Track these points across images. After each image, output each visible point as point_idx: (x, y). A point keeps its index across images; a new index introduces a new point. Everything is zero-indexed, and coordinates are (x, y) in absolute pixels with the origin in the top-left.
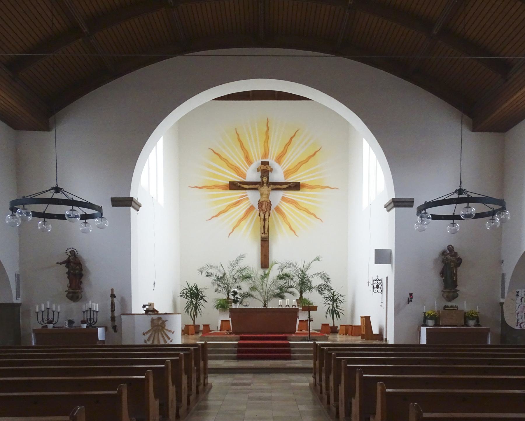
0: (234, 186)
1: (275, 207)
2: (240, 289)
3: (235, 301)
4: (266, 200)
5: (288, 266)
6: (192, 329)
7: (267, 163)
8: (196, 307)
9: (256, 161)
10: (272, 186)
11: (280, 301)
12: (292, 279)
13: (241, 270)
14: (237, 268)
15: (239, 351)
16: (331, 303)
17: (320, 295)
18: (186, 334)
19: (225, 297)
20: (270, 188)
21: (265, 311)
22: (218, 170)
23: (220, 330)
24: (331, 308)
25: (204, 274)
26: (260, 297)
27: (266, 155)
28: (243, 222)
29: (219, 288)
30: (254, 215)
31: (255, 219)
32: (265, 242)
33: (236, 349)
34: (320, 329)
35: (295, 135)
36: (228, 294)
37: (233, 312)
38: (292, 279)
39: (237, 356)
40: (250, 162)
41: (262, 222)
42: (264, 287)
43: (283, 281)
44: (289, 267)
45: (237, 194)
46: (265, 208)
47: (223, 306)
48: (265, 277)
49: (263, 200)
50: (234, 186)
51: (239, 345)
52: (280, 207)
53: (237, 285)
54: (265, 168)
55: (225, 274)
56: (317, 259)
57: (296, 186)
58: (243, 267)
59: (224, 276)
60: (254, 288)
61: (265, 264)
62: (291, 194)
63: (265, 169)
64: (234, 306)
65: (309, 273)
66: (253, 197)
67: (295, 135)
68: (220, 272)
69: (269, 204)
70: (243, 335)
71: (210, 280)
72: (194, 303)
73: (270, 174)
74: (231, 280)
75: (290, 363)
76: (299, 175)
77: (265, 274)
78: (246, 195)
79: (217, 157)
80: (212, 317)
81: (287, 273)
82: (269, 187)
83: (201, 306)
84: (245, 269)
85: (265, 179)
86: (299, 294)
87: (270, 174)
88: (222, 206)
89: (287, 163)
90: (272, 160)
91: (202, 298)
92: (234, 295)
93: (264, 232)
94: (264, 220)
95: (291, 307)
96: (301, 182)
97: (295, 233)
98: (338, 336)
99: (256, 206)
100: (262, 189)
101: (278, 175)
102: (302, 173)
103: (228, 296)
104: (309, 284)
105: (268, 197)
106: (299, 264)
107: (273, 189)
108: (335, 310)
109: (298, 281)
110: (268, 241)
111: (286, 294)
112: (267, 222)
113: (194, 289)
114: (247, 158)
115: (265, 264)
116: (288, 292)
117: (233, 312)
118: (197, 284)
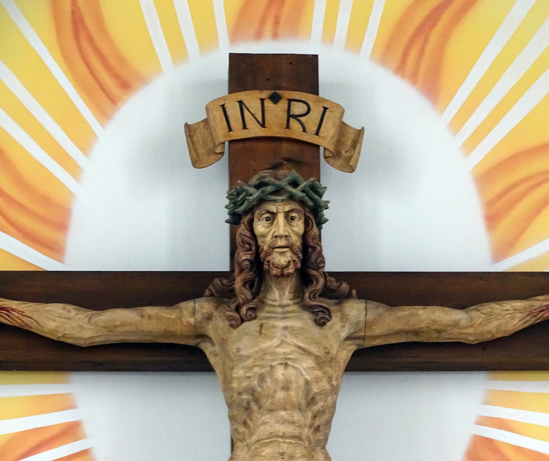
7: (302, 72)
10: (355, 310)
40: (107, 76)
54: (275, 129)
63: (275, 138)
73: (333, 181)
78: (70, 431)
82: (322, 319)
85: (278, 229)
90: (354, 43)
100: (245, 342)
107: (372, 359)
114: (78, 22)
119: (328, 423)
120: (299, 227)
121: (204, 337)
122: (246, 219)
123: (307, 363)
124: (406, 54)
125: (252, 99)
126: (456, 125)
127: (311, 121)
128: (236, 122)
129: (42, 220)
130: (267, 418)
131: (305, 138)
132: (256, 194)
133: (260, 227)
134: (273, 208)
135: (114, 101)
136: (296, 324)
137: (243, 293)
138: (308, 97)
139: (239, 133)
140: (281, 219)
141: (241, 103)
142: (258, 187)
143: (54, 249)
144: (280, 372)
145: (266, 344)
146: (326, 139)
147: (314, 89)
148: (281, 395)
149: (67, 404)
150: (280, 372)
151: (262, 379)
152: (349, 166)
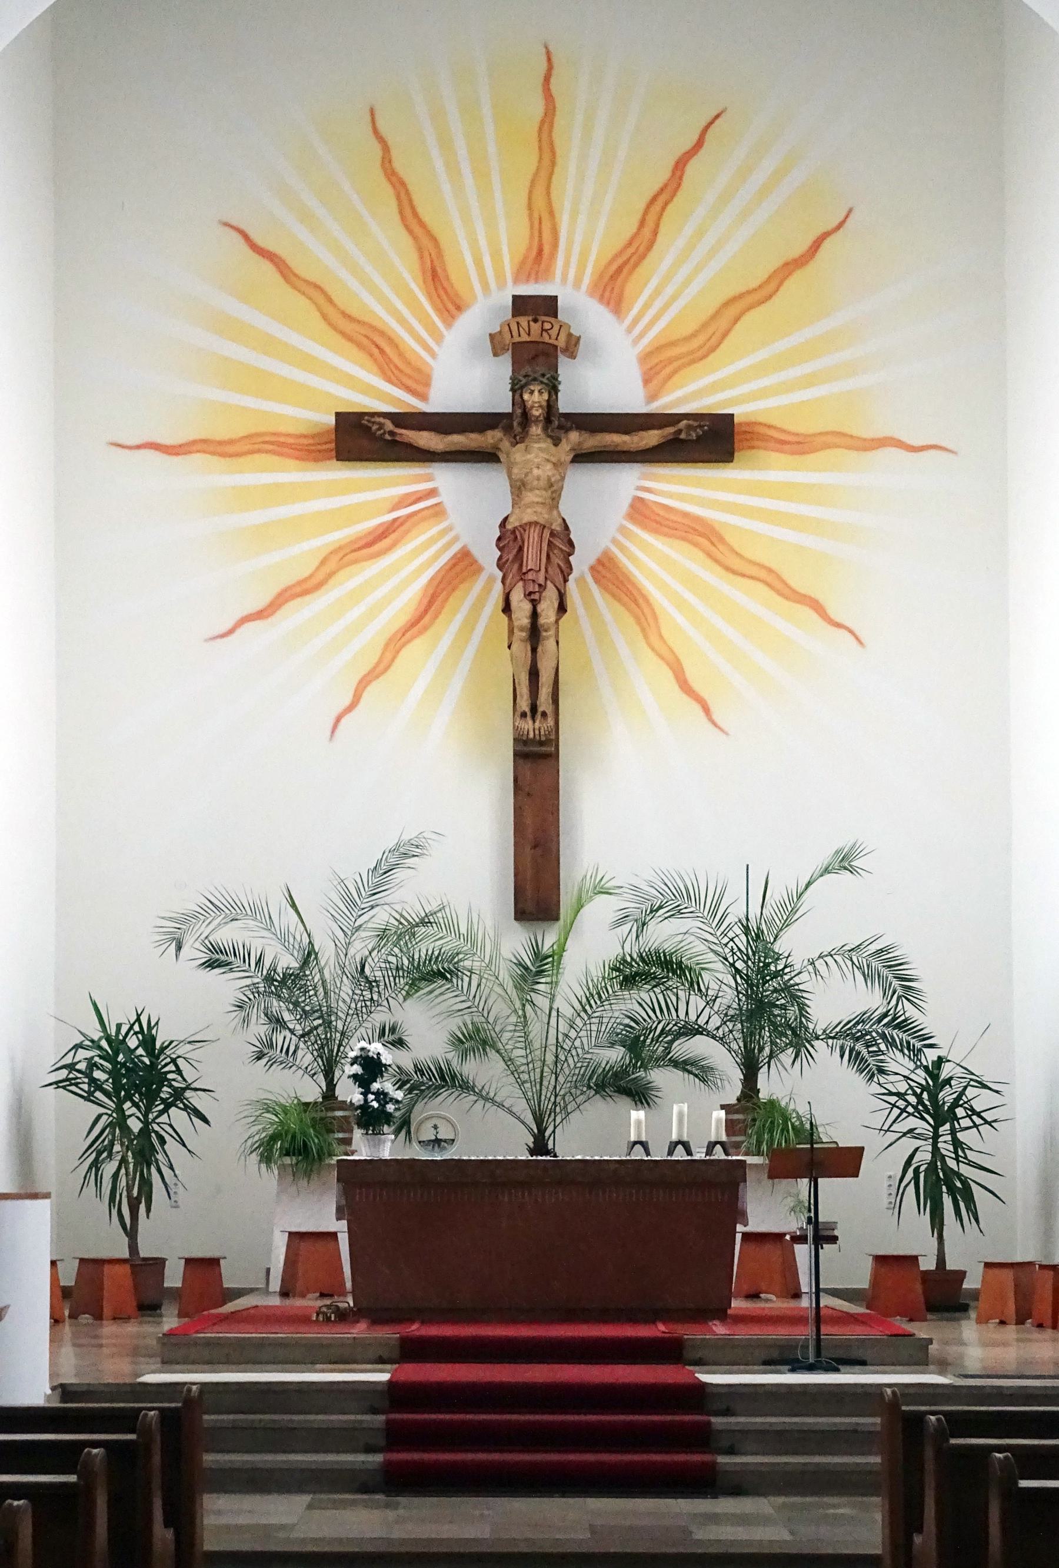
0: (360, 439)
1: (592, 561)
2: (400, 1043)
3: (372, 1119)
4: (543, 516)
5: (674, 902)
6: (116, 1281)
7: (548, 306)
8: (145, 1150)
10: (574, 436)
11: (638, 1115)
12: (694, 985)
13: (406, 931)
14: (381, 917)
15: (396, 1437)
16: (922, 1127)
17: (860, 1080)
18: (85, 1318)
19: (312, 1091)
20: (565, 446)
21: (541, 1176)
22: (268, 345)
23: (284, 1294)
24: (925, 1156)
25: (194, 951)
26: (508, 1091)
27: (538, 258)
28: (416, 648)
29: (278, 1038)
30: (469, 625)
31: (480, 629)
32: (536, 764)
33: (379, 1419)
34: (865, 1284)
35: (699, 144)
36: (329, 1074)
37: (360, 1183)
38: (694, 985)
39: (388, 1465)
40: (449, 302)
41: (521, 649)
42: (536, 1029)
43: (645, 994)
44: (678, 912)
45: (378, 488)
46: (535, 563)
47: (297, 1144)
48: (538, 969)
49: (528, 516)
50: (360, 439)
51: (396, 1395)
53: (380, 1017)
54: (535, 336)
55: (309, 956)
56: (844, 862)
57: (711, 439)
58: (415, 912)
59: (305, 963)
60: (475, 1040)
61: (537, 893)
62: (679, 486)
63: (535, 341)
64: (363, 1148)
65: (795, 946)
66: (469, 503)
67: (699, 144)
68: (283, 940)
69: (561, 542)
70: (415, 1329)
71: (228, 987)
72: (135, 1125)
74: (347, 988)
75: (714, 1519)
76: (731, 369)
77: (539, 957)
78: (432, 493)
79: (267, 266)
80: (239, 1210)
81: (668, 947)
82: (556, 442)
83: (171, 1145)
84: (424, 922)
85: (535, 398)
86: (736, 1075)
87: (566, 369)
88: (301, 555)
89: (658, 304)
90: (577, 285)
91: (178, 1095)
92: (363, 1081)
93: (534, 709)
94: (535, 633)
95: (659, 1154)
96: (740, 412)
97: (707, 710)
98: (969, 1329)
99: (488, 555)
100: (518, 454)
101: (605, 378)
102: (741, 364)
103: (331, 1085)
104: (792, 1012)
105: (554, 501)
106: (735, 892)
107: (582, 457)
108: (945, 1168)
109: (728, 997)
110: (554, 756)
111: (660, 1077)
112: (548, 645)
113: (132, 1042)
115: (537, 893)
116: (676, 1064)
117: (360, 1183)
118: (152, 1012)
119: (560, 495)
120: (546, 396)
121: (499, 449)
122: (519, 392)
123: (549, 466)
124: (604, 291)
125: (524, 321)
126: (629, 330)
127: (554, 332)
128: (515, 333)
129: (416, 381)
130: (529, 494)
131: (550, 341)
132: (524, 381)
133: (526, 397)
134: (532, 388)
135: (453, 317)
136: (543, 445)
137: (517, 428)
138: (552, 320)
139: (517, 339)
140: (536, 393)
141: (518, 323)
142: (525, 376)
143: (423, 397)
144: (536, 472)
145: (529, 456)
146: (561, 342)
147: (556, 316)
148: (535, 483)
149: (430, 478)
150: (536, 472)
151: (526, 475)
152: (573, 356)
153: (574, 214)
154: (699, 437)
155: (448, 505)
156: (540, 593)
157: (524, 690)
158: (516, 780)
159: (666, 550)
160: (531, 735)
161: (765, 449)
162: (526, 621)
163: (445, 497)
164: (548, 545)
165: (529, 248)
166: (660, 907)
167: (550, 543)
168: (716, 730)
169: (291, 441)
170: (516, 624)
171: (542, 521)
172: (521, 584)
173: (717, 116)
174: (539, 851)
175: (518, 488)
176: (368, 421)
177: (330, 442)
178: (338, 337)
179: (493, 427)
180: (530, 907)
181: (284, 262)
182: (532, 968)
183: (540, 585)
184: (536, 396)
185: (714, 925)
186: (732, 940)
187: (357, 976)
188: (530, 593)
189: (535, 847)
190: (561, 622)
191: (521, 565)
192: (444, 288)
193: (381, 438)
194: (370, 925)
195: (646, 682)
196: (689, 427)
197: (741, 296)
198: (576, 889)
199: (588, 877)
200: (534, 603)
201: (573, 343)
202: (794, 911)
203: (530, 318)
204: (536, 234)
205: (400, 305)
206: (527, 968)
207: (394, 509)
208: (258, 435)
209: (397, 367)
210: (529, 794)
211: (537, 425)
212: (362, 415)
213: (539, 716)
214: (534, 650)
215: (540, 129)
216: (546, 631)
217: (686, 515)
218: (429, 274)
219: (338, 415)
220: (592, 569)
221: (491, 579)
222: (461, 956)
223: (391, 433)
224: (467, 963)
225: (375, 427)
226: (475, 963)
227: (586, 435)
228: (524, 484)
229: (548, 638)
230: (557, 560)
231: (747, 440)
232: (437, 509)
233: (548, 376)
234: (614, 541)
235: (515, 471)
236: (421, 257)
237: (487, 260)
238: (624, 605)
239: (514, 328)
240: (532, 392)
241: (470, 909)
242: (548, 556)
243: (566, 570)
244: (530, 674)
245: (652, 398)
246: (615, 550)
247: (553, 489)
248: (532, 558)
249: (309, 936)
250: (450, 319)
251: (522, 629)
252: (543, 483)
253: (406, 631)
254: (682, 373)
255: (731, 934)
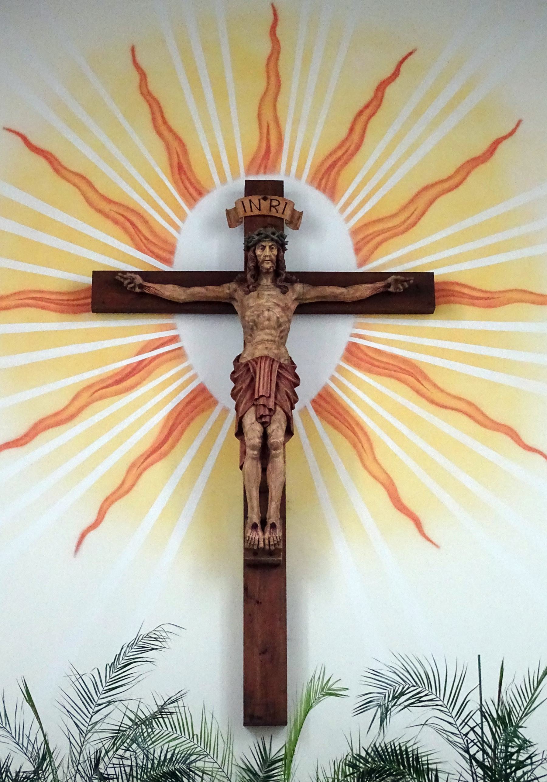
0: (114, 294)
1: (313, 395)
9: (224, 181)
10: (299, 287)
14: (115, 717)
20: (291, 296)
22: (41, 223)
27: (267, 155)
28: (156, 472)
32: (265, 575)
41: (252, 467)
45: (128, 335)
46: (265, 393)
50: (114, 294)
52: (339, 392)
57: (415, 295)
58: (149, 708)
61: (266, 697)
62: (388, 334)
63: (264, 215)
66: (206, 348)
69: (287, 375)
77: (268, 762)
78: (174, 339)
79: (42, 163)
82: (284, 292)
85: (266, 253)
88: (56, 391)
90: (299, 176)
93: (263, 522)
96: (440, 273)
99: (222, 388)
100: (251, 301)
101: (325, 243)
107: (305, 309)
114: (180, 167)
115: (266, 697)
119: (287, 335)
120: (275, 252)
121: (234, 299)
122: (252, 249)
123: (277, 310)
125: (255, 199)
127: (280, 208)
130: (260, 332)
131: (277, 215)
132: (257, 238)
133: (258, 252)
134: (264, 244)
135: (195, 200)
136: (272, 293)
139: (249, 213)
140: (267, 248)
141: (250, 201)
144: (266, 314)
146: (287, 216)
148: (266, 323)
149: (173, 327)
150: (266, 314)
151: (258, 316)
153: (296, 122)
154: (405, 290)
155: (188, 350)
156: (271, 416)
157: (255, 503)
158: (246, 589)
159: (378, 386)
160: (262, 545)
161: (460, 303)
162: (257, 441)
163: (184, 343)
164: (278, 375)
165: (259, 147)
166: (402, 694)
167: (279, 375)
168: (428, 543)
169: (53, 297)
170: (248, 443)
171: (272, 355)
172: (253, 409)
173: (410, 54)
174: (267, 656)
175: (250, 330)
176: (121, 277)
177: (88, 298)
178: (97, 216)
179: (230, 281)
180: (259, 711)
181: (56, 159)
182: (261, 774)
183: (270, 410)
184: (267, 251)
185: (454, 714)
186: (472, 729)
187: (90, 772)
188: (262, 417)
189: (263, 652)
190: (287, 444)
191: (253, 394)
192: (189, 180)
193: (131, 292)
194: (105, 726)
195: (365, 500)
196: (396, 281)
197: (432, 185)
198: (305, 689)
199: (317, 678)
200: (265, 425)
201: (296, 218)
202: (532, 701)
203: (262, 196)
204: (265, 139)
205: (152, 192)
206: (255, 774)
207: (139, 353)
208: (23, 292)
209: (146, 238)
210: (258, 602)
211: (267, 279)
212: (116, 273)
213: (268, 529)
214: (264, 470)
215: (268, 65)
216: (276, 449)
217: (394, 357)
218: (176, 169)
219: (95, 274)
220: (314, 402)
221: (225, 411)
222: (193, 758)
223: (141, 286)
224: (199, 764)
225: (126, 282)
226: (207, 765)
227: (308, 288)
228: (255, 324)
229: (276, 456)
230: (284, 387)
231: (444, 296)
232: (179, 351)
233: (277, 234)
234: (333, 379)
235: (248, 313)
236: (170, 154)
237: (224, 158)
238: (341, 432)
239: (247, 203)
240: (264, 248)
241: (203, 713)
242: (277, 385)
243: (293, 399)
244: (260, 492)
245: (360, 265)
246: (332, 385)
247: (282, 328)
248: (263, 386)
249: (45, 736)
250: (192, 201)
251: (253, 448)
252: (273, 323)
253: (149, 456)
254: (384, 245)
255: (472, 724)
